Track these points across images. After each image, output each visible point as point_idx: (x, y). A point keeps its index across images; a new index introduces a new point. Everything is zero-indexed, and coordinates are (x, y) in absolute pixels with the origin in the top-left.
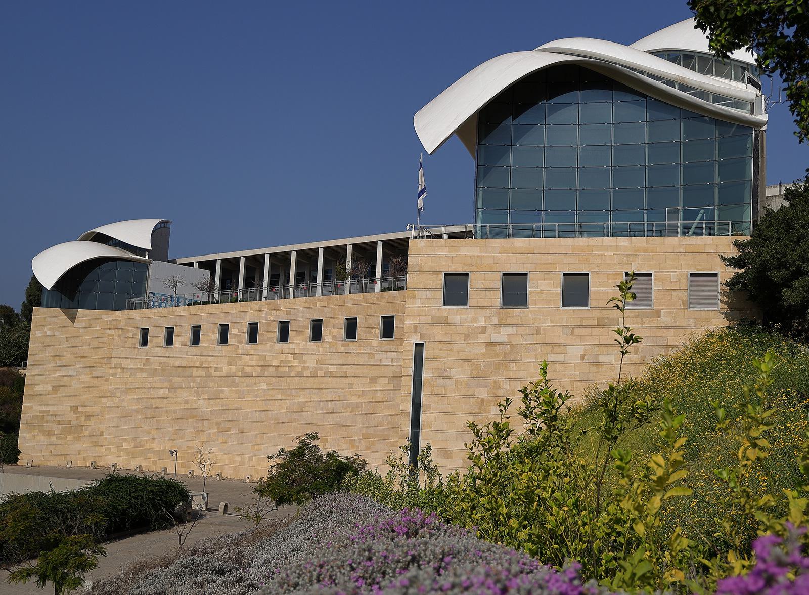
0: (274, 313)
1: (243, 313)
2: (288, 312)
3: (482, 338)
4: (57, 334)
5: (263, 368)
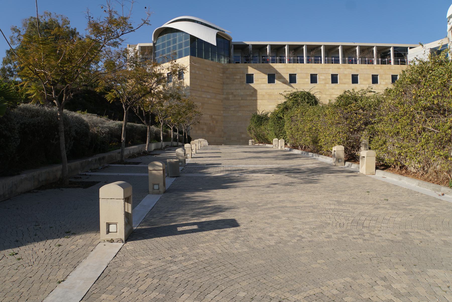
2: (357, 70)
4: (201, 73)
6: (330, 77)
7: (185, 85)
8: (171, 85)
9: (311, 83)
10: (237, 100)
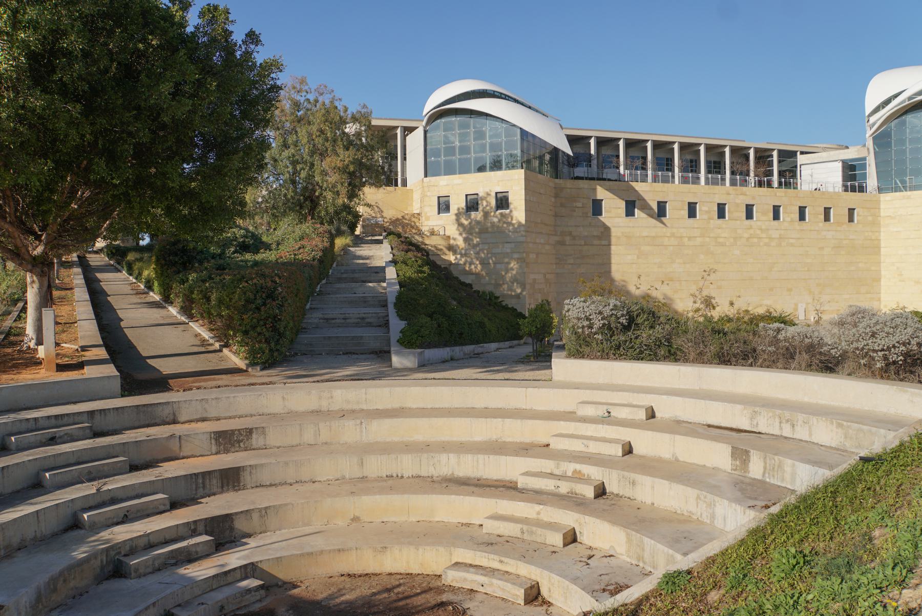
2: (754, 198)
6: (716, 208)
7: (514, 222)
9: (689, 217)
10: (577, 245)
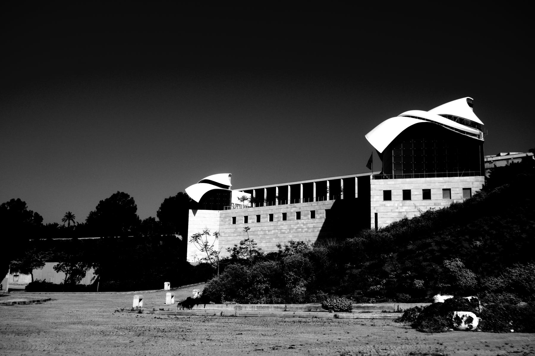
0: (294, 209)
1: (280, 209)
2: (300, 208)
3: (397, 210)
5: (290, 229)
8: (478, 242)
